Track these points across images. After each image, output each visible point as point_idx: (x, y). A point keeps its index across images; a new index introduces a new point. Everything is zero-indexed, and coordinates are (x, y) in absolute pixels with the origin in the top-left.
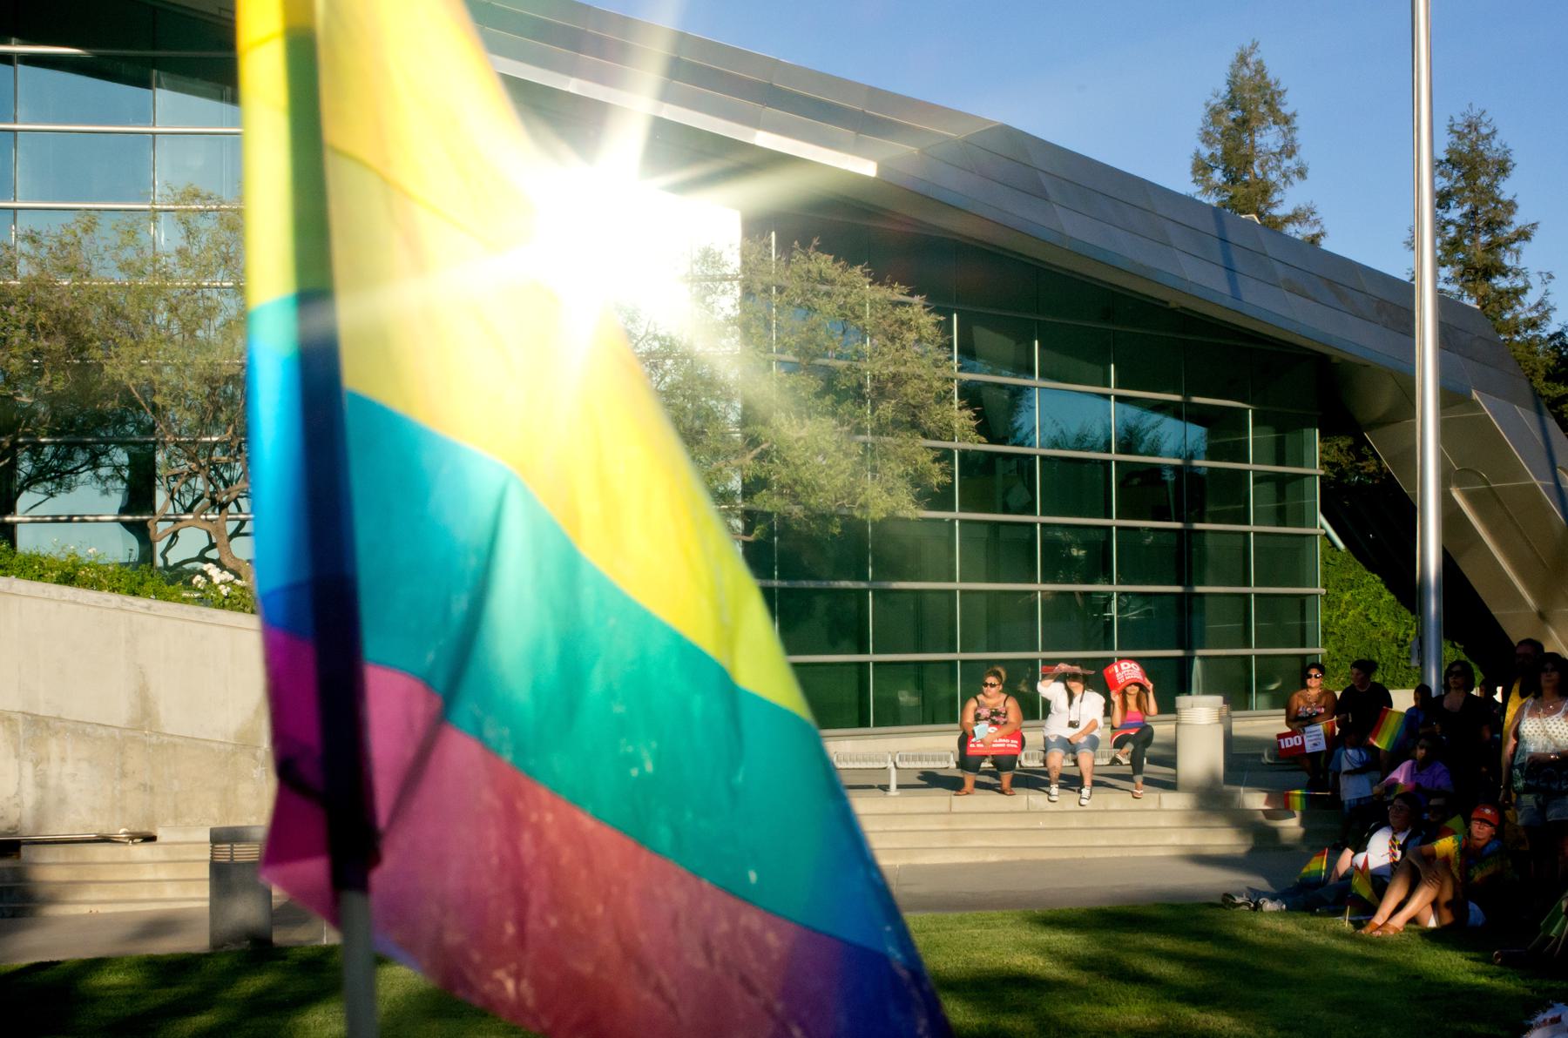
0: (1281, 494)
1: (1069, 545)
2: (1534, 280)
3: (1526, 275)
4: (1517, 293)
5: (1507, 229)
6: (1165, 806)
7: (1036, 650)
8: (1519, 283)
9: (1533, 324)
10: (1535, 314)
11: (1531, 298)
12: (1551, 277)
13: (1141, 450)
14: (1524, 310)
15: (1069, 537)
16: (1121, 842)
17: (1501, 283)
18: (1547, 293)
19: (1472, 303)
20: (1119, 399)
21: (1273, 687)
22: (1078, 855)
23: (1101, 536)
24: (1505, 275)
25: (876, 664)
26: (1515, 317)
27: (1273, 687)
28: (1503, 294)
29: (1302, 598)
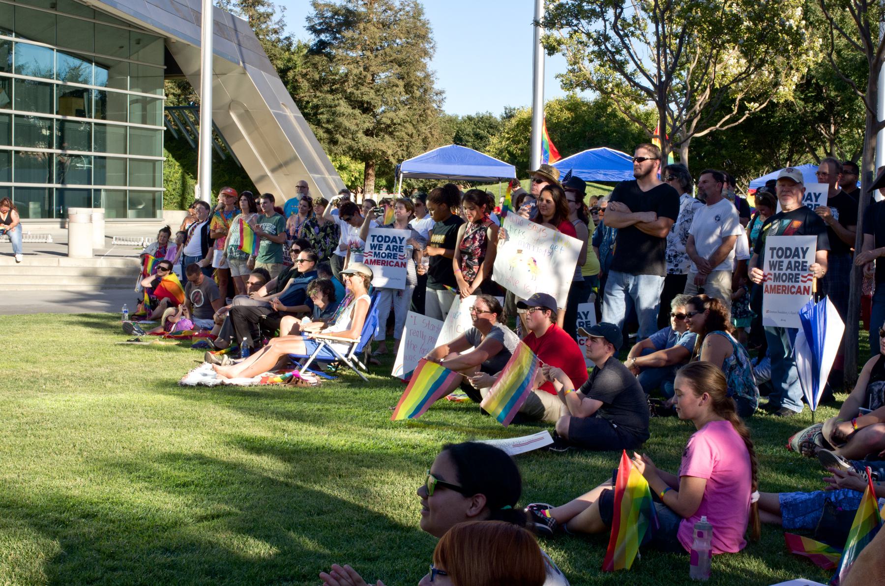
0: (144, 109)
1: (41, 128)
2: (277, 10)
3: (273, 6)
4: (269, 16)
5: (641, 106)
6: (61, 265)
7: (11, 181)
8: (270, 10)
9: (276, 32)
10: (277, 26)
11: (275, 18)
12: (285, 9)
13: (80, 79)
14: (272, 24)
15: (41, 123)
16: (37, 283)
17: (261, 9)
18: (283, 16)
19: (245, 18)
20: (57, 51)
21: (141, 207)
22: (14, 289)
23: (6, 119)
24: (263, 5)
25: (16, 188)
26: (267, 28)
27: (141, 207)
28: (261, 15)
29: (154, 162)
